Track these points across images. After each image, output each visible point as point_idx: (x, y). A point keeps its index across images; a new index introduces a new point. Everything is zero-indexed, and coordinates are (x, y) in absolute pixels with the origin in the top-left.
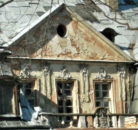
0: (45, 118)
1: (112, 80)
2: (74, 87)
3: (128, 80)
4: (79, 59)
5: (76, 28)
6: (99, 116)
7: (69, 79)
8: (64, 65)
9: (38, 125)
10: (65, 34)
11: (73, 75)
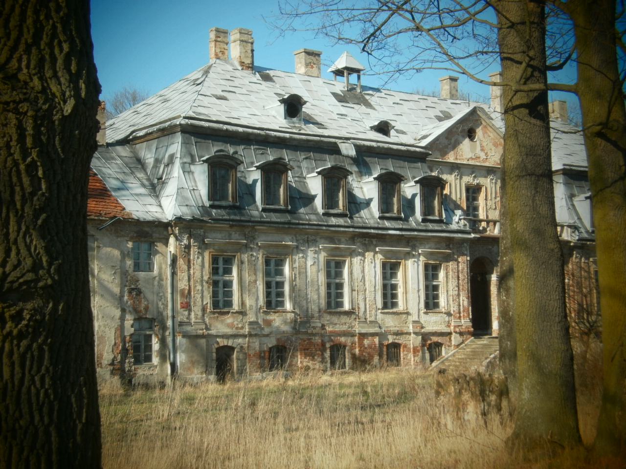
0: (466, 222)
2: (482, 193)
4: (487, 164)
5: (485, 133)
7: (478, 184)
8: (473, 169)
9: (459, 228)
10: (474, 138)
11: (481, 180)
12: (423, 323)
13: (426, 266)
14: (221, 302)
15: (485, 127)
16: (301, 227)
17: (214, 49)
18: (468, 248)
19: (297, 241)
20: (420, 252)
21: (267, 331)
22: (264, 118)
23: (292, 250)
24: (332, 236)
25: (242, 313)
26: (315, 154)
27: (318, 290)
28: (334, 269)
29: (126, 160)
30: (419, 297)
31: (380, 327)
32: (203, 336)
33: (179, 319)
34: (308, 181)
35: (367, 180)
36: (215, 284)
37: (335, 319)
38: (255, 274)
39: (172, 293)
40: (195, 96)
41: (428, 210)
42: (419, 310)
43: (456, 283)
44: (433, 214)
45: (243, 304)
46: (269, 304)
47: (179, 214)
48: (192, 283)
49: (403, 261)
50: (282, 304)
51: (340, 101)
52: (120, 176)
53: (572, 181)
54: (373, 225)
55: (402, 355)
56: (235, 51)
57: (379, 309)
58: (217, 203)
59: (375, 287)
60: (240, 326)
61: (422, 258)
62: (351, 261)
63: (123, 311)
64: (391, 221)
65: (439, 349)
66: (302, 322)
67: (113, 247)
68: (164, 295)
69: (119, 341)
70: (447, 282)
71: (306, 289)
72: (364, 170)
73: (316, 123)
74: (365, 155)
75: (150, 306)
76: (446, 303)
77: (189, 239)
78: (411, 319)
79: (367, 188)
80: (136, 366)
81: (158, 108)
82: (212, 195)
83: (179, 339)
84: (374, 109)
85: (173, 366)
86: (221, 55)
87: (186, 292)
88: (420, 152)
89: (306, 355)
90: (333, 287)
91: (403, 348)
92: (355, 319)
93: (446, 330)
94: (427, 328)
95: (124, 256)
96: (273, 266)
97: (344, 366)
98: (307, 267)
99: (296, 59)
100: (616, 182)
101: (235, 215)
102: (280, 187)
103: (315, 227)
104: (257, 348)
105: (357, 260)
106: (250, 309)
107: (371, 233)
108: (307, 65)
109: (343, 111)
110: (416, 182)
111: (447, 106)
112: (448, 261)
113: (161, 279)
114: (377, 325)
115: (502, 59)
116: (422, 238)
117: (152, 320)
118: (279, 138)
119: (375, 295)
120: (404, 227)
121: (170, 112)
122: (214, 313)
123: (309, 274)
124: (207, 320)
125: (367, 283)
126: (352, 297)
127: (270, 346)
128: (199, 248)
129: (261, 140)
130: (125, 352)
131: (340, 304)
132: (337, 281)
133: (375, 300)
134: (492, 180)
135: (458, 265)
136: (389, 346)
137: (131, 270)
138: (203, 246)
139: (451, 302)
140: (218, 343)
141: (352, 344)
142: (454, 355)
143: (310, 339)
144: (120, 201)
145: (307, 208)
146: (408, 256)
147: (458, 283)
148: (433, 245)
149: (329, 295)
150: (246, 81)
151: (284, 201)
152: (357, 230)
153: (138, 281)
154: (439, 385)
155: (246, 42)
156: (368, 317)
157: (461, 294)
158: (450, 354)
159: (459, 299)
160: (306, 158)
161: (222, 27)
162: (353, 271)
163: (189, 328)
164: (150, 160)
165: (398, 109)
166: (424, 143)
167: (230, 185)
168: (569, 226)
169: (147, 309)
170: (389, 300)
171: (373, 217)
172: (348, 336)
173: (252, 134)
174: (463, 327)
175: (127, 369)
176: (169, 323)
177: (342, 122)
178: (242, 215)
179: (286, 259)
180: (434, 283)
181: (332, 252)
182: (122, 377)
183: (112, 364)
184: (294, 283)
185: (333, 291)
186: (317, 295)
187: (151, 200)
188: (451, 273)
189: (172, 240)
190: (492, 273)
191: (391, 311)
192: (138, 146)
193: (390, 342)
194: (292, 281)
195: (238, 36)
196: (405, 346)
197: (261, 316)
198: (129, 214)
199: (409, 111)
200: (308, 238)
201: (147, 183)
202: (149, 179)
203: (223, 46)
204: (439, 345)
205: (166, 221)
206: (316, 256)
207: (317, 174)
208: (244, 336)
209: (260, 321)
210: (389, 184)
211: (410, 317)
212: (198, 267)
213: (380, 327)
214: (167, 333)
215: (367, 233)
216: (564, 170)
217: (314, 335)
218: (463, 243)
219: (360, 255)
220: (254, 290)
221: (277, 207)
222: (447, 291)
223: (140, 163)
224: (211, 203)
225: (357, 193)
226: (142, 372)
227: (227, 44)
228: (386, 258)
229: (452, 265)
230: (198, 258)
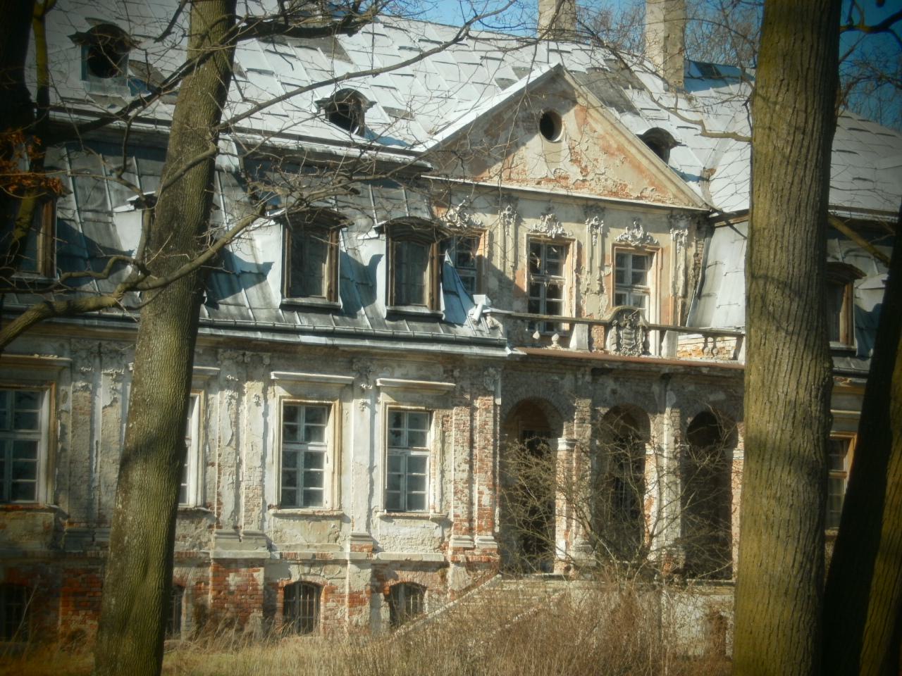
0: (496, 322)
1: (657, 247)
2: (569, 256)
3: (692, 251)
6: (619, 327)
7: (558, 237)
8: (550, 204)
9: (479, 335)
11: (569, 229)
12: (378, 539)
13: (396, 418)
18: (498, 377)
20: (379, 384)
23: (60, 373)
26: (142, 161)
30: (372, 483)
31: (270, 547)
34: (116, 220)
41: (403, 291)
42: (370, 510)
43: (465, 455)
49: (337, 402)
50: (29, 492)
54: (261, 323)
55: (322, 608)
57: (270, 507)
59: (263, 458)
61: (384, 398)
62: (207, 400)
64: (311, 315)
65: (415, 598)
70: (443, 452)
71: (90, 458)
76: (438, 498)
91: (326, 594)
92: (211, 526)
93: (437, 557)
94: (388, 552)
103: (116, 324)
105: (220, 399)
107: (256, 339)
114: (264, 542)
116: (385, 355)
119: (263, 476)
120: (338, 328)
125: (244, 450)
126: (204, 479)
133: (263, 486)
135: (472, 415)
136: (290, 590)
139: (450, 496)
141: (199, 583)
143: (90, 571)
146: (349, 390)
147: (471, 454)
148: (412, 369)
151: (44, 263)
152: (222, 332)
156: (242, 522)
157: (477, 477)
158: (438, 612)
159: (471, 491)
162: (212, 423)
171: (268, 305)
172: (190, 565)
174: (477, 552)
179: (43, 391)
180: (414, 453)
184: (60, 446)
188: (453, 433)
190: (560, 436)
193: (293, 580)
196: (332, 590)
200: (100, 346)
207: (132, 207)
210: (309, 236)
211: (346, 526)
213: (270, 547)
215: (249, 340)
218: (486, 368)
219: (229, 388)
222: (442, 472)
228: (295, 396)
229: (457, 415)
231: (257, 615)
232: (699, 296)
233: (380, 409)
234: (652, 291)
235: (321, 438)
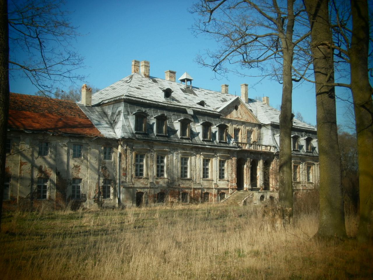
1: (253, 130)
3: (258, 131)
4: (242, 120)
5: (241, 108)
6: (254, 145)
7: (239, 128)
14: (139, 173)
15: (242, 105)
16: (172, 143)
17: (133, 69)
19: (170, 149)
21: (157, 186)
22: (156, 98)
24: (184, 147)
25: (147, 178)
27: (178, 170)
28: (184, 161)
29: (100, 112)
31: (202, 186)
32: (131, 188)
33: (122, 180)
34: (174, 124)
35: (197, 125)
36: (137, 166)
37: (184, 182)
38: (153, 162)
39: (119, 169)
40: (128, 87)
41: (221, 138)
44: (223, 140)
45: (147, 175)
46: (158, 175)
47: (123, 136)
48: (127, 165)
50: (163, 175)
51: (184, 92)
52: (98, 119)
53: (274, 129)
55: (209, 197)
56: (142, 70)
58: (138, 132)
60: (146, 184)
61: (218, 158)
63: (99, 176)
66: (171, 183)
67: (96, 149)
68: (116, 170)
69: (97, 188)
72: (196, 121)
73: (176, 100)
74: (197, 115)
75: (110, 174)
77: (127, 146)
78: (214, 182)
79: (197, 128)
80: (104, 199)
81: (111, 92)
82: (136, 129)
83: (122, 188)
84: (197, 96)
85: (119, 199)
86: (137, 71)
87: (125, 169)
88: (218, 114)
89: (172, 197)
90: (183, 168)
95: (100, 153)
96: (160, 160)
97: (187, 201)
98: (173, 160)
99: (166, 74)
100: (369, 127)
101: (146, 137)
102: (163, 126)
104: (153, 193)
105: (193, 158)
106: (150, 177)
108: (170, 77)
109: (186, 96)
110: (217, 126)
111: (224, 96)
112: (228, 159)
113: (115, 163)
115: (315, 72)
117: (111, 180)
118: (163, 106)
120: (212, 144)
121: (117, 94)
122: (136, 178)
123: (174, 163)
124: (133, 181)
125: (197, 167)
127: (158, 192)
128: (130, 151)
129: (155, 106)
130: (99, 193)
131: (186, 176)
132: (185, 166)
134: (244, 127)
137: (103, 159)
138: (132, 150)
139: (229, 176)
140: (137, 191)
142: (229, 198)
143: (174, 190)
144: (99, 130)
145: (174, 135)
146: (213, 156)
149: (182, 172)
150: (147, 82)
152: (194, 145)
153: (105, 163)
154: (265, 212)
155: (147, 66)
160: (173, 115)
161: (137, 60)
163: (126, 184)
164: (110, 113)
165: (206, 96)
166: (219, 110)
167: (144, 125)
168: (273, 147)
169: (109, 175)
170: (205, 175)
171: (200, 140)
173: (152, 104)
175: (100, 200)
176: (118, 181)
177: (187, 101)
178: (148, 137)
180: (223, 168)
181: (183, 154)
182: (99, 204)
183: (94, 198)
185: (183, 170)
186: (177, 172)
187: (111, 130)
189: (120, 147)
190: (245, 164)
191: (206, 179)
192: (104, 107)
194: (168, 165)
195: (144, 64)
196: (211, 194)
197: (155, 180)
198: (103, 135)
199: (211, 98)
201: (108, 122)
202: (109, 121)
203: (137, 67)
204: (224, 194)
205: (117, 139)
206: (177, 155)
208: (148, 188)
209: (154, 182)
210: (206, 126)
212: (130, 159)
213: (202, 186)
214: (117, 186)
215: (198, 147)
216: (271, 124)
217: (176, 188)
220: (152, 169)
221: (162, 134)
223: (105, 114)
224: (136, 132)
225: (193, 130)
226: (106, 201)
227: (139, 67)
229: (230, 161)
230: (130, 155)
231: (200, 199)
232: (260, 139)
233: (218, 160)
234: (252, 138)
235: (208, 165)
